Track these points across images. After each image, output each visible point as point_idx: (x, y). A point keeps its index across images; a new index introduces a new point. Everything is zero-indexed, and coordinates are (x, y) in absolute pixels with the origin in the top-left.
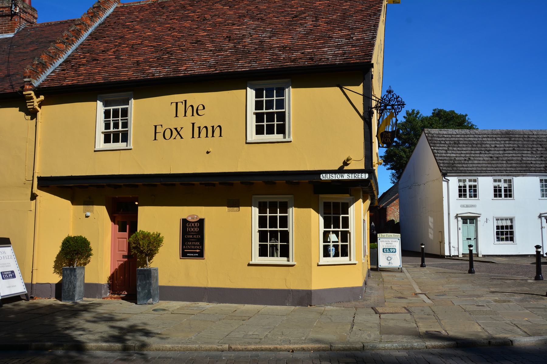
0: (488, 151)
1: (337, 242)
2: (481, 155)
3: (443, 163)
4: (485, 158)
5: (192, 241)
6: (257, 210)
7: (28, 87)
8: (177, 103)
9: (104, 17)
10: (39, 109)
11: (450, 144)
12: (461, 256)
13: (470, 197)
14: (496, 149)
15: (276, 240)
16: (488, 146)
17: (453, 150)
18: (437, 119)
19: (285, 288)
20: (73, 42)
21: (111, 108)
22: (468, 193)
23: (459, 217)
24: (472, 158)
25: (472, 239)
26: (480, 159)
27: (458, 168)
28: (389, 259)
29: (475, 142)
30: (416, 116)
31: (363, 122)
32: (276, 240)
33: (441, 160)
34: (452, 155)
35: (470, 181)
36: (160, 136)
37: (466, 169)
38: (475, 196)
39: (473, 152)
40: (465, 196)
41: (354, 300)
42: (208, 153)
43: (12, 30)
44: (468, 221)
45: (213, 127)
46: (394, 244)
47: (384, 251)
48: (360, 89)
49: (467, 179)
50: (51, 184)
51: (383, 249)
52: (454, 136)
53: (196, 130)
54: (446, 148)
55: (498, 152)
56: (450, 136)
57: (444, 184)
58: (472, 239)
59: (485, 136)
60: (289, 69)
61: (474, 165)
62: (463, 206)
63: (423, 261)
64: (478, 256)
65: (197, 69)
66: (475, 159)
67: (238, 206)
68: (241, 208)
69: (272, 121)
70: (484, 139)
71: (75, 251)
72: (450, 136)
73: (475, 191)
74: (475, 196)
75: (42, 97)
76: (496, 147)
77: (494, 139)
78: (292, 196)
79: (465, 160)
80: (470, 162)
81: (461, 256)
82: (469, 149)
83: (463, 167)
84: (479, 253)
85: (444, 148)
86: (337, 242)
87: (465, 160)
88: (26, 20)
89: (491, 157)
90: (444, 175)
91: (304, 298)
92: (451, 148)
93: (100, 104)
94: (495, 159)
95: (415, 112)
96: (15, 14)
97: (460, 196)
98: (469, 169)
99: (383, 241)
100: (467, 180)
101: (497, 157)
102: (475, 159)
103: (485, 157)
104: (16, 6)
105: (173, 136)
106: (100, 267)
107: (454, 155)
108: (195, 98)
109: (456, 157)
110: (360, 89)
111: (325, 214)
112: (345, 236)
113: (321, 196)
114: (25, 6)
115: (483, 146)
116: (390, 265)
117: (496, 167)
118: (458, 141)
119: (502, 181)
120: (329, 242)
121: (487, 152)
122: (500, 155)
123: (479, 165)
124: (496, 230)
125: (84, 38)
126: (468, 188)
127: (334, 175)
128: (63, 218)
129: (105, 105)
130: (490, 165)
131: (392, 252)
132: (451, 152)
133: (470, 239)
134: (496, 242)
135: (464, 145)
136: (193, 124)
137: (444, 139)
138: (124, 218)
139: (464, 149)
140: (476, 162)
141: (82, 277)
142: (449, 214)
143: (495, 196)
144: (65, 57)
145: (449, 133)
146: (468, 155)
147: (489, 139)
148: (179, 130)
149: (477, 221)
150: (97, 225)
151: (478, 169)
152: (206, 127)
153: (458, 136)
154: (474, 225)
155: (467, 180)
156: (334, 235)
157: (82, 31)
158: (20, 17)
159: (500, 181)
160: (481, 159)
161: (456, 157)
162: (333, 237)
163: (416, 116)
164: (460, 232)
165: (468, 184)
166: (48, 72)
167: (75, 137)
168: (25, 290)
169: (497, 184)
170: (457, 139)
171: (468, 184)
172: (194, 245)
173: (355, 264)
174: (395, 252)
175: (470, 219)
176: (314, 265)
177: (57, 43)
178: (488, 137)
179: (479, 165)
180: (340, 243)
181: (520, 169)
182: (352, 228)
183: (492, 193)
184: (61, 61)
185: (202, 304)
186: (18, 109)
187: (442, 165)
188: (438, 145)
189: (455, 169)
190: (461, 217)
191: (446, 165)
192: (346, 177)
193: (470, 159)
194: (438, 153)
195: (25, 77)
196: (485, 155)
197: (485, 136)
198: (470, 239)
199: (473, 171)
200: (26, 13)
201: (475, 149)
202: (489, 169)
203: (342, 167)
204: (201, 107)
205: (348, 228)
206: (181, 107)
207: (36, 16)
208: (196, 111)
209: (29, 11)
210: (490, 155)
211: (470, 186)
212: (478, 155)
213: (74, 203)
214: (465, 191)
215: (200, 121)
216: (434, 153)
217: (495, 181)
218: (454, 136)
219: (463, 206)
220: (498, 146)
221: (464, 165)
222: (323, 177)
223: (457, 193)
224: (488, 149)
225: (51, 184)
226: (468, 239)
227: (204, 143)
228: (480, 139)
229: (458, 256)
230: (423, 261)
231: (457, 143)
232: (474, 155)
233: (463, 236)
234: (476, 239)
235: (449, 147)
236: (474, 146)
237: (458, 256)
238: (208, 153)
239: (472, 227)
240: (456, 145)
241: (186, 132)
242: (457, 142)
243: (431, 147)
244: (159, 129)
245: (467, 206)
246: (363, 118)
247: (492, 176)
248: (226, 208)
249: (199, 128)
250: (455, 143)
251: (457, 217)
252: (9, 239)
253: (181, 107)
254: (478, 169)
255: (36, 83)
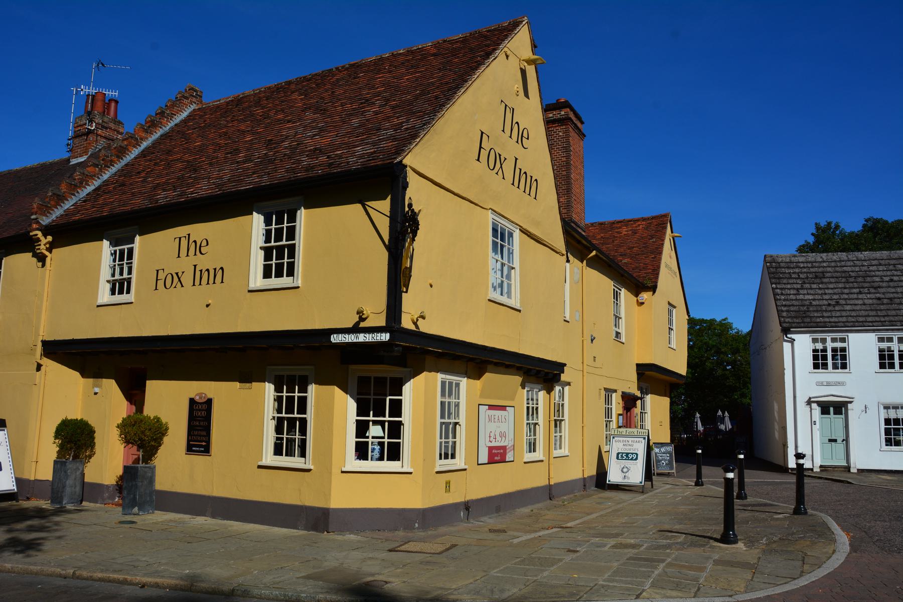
0: (875, 288)
1: (383, 438)
2: (860, 296)
3: (788, 311)
4: (866, 301)
5: (198, 430)
6: (272, 387)
7: (34, 226)
8: (180, 238)
9: (171, 124)
10: (47, 253)
11: (807, 278)
12: (817, 469)
13: (835, 367)
14: (891, 284)
15: (291, 433)
16: (877, 279)
17: (811, 289)
18: (870, 234)
19: (299, 503)
20: (112, 163)
21: (118, 248)
22: (830, 362)
23: (814, 402)
24: (843, 302)
25: (840, 440)
26: (857, 302)
27: (813, 320)
28: (625, 470)
29: (853, 274)
30: (834, 232)
31: (387, 254)
32: (291, 433)
33: (785, 306)
34: (807, 297)
35: (834, 340)
36: (161, 283)
37: (827, 320)
38: (844, 366)
39: (846, 291)
40: (825, 366)
41: (405, 529)
42: (208, 306)
43: (86, 153)
44: (832, 409)
45: (215, 269)
46: (636, 446)
47: (617, 458)
48: (385, 205)
49: (828, 337)
50: (58, 350)
51: (618, 454)
52: (817, 265)
53: (198, 273)
54: (799, 286)
55: (893, 290)
56: (810, 265)
57: (787, 346)
58: (840, 440)
59: (874, 262)
60: (271, 187)
61: (844, 314)
62: (820, 384)
63: (699, 475)
64: (849, 471)
65: (203, 189)
66: (849, 302)
67: (251, 382)
68: (254, 383)
69: (280, 258)
70: (871, 268)
71: (76, 438)
72: (810, 265)
73: (844, 357)
74: (844, 366)
75: (50, 238)
76: (892, 280)
77: (891, 267)
78: (312, 367)
79: (829, 305)
80: (837, 308)
81: (817, 469)
82: (840, 285)
83: (823, 317)
84: (852, 465)
85: (795, 286)
86: (383, 438)
87: (829, 305)
88: (105, 138)
89: (879, 299)
90: (786, 331)
91: (319, 519)
92: (807, 286)
93: (106, 243)
94: (885, 301)
95: (833, 225)
96: (90, 132)
97: (816, 366)
98: (833, 320)
99: (619, 441)
100: (829, 339)
101: (891, 299)
102: (849, 302)
103: (868, 298)
104: (91, 121)
105: (174, 285)
106: (108, 461)
107: (811, 297)
108: (199, 231)
109: (814, 300)
110: (385, 205)
111: (358, 394)
112: (395, 430)
113: (353, 367)
114: (106, 119)
115: (869, 279)
116: (626, 480)
117: (884, 316)
118: (823, 272)
119: (895, 340)
120: (368, 437)
121: (872, 290)
122: (896, 295)
123: (853, 314)
124: (883, 426)
125: (133, 156)
126: (829, 354)
127: (347, 336)
128: (71, 394)
129: (114, 244)
130: (874, 313)
131: (632, 459)
132: (805, 292)
133: (835, 441)
134: (885, 448)
135: (833, 280)
136: (195, 266)
137: (797, 270)
138: (134, 393)
139: (831, 286)
140: (848, 307)
141: (78, 473)
142: (795, 397)
143: (882, 366)
144: (97, 183)
145: (810, 259)
146: (835, 297)
147: (881, 268)
148: (180, 275)
149: (847, 410)
150: (102, 404)
151: (850, 319)
152: (208, 270)
153: (825, 264)
154: (843, 416)
155: (829, 339)
156: (379, 427)
157: (130, 148)
158: (97, 135)
159: (890, 340)
160: (860, 302)
161: (814, 300)
162: (375, 431)
163: (834, 232)
164: (816, 428)
165: (830, 345)
166: (68, 205)
167: (84, 287)
168: (15, 488)
169: (885, 345)
170: (821, 270)
171: (830, 345)
172: (200, 436)
173: (411, 473)
174: (636, 459)
175: (834, 408)
176: (336, 471)
177: (88, 166)
178: (880, 265)
179: (853, 314)
180: (386, 440)
181: (873, 319)
182: (406, 417)
183: (876, 361)
184: (90, 189)
185: (200, 520)
186: (31, 254)
187: (784, 314)
188: (785, 281)
189: (808, 320)
190: (817, 402)
191: (793, 314)
192: (362, 338)
193: (838, 303)
194: (782, 294)
195: (32, 214)
196: (868, 296)
197: (874, 262)
198: (835, 441)
199: (839, 324)
200: (106, 128)
201: (851, 285)
202: (870, 319)
203: (358, 323)
204: (204, 243)
205: (401, 417)
206: (184, 242)
207: (121, 130)
208: (199, 250)
209: (112, 125)
210: (878, 295)
211: (834, 350)
212: (855, 296)
213: (84, 375)
214: (825, 358)
215: (204, 262)
216: (775, 295)
217: (881, 340)
218: (817, 265)
219: (820, 384)
220: (895, 278)
221: (825, 314)
222: (336, 339)
223: (810, 362)
224: (876, 284)
225: (58, 350)
226: (830, 441)
227: (206, 292)
228: (865, 268)
229: (812, 470)
230: (699, 475)
231: (819, 277)
232: (846, 296)
233: (822, 435)
234: (846, 440)
235: (804, 283)
236: (852, 280)
237: (812, 470)
238: (208, 306)
239: (839, 419)
240: (818, 281)
241: (187, 279)
242: (821, 275)
243: (772, 284)
244: (162, 275)
245: (828, 384)
246: (388, 248)
247: (874, 331)
248: (237, 385)
249: (201, 271)
250: (816, 277)
251: (809, 402)
252: (4, 420)
253: (184, 242)
254: (850, 319)
255: (45, 221)
